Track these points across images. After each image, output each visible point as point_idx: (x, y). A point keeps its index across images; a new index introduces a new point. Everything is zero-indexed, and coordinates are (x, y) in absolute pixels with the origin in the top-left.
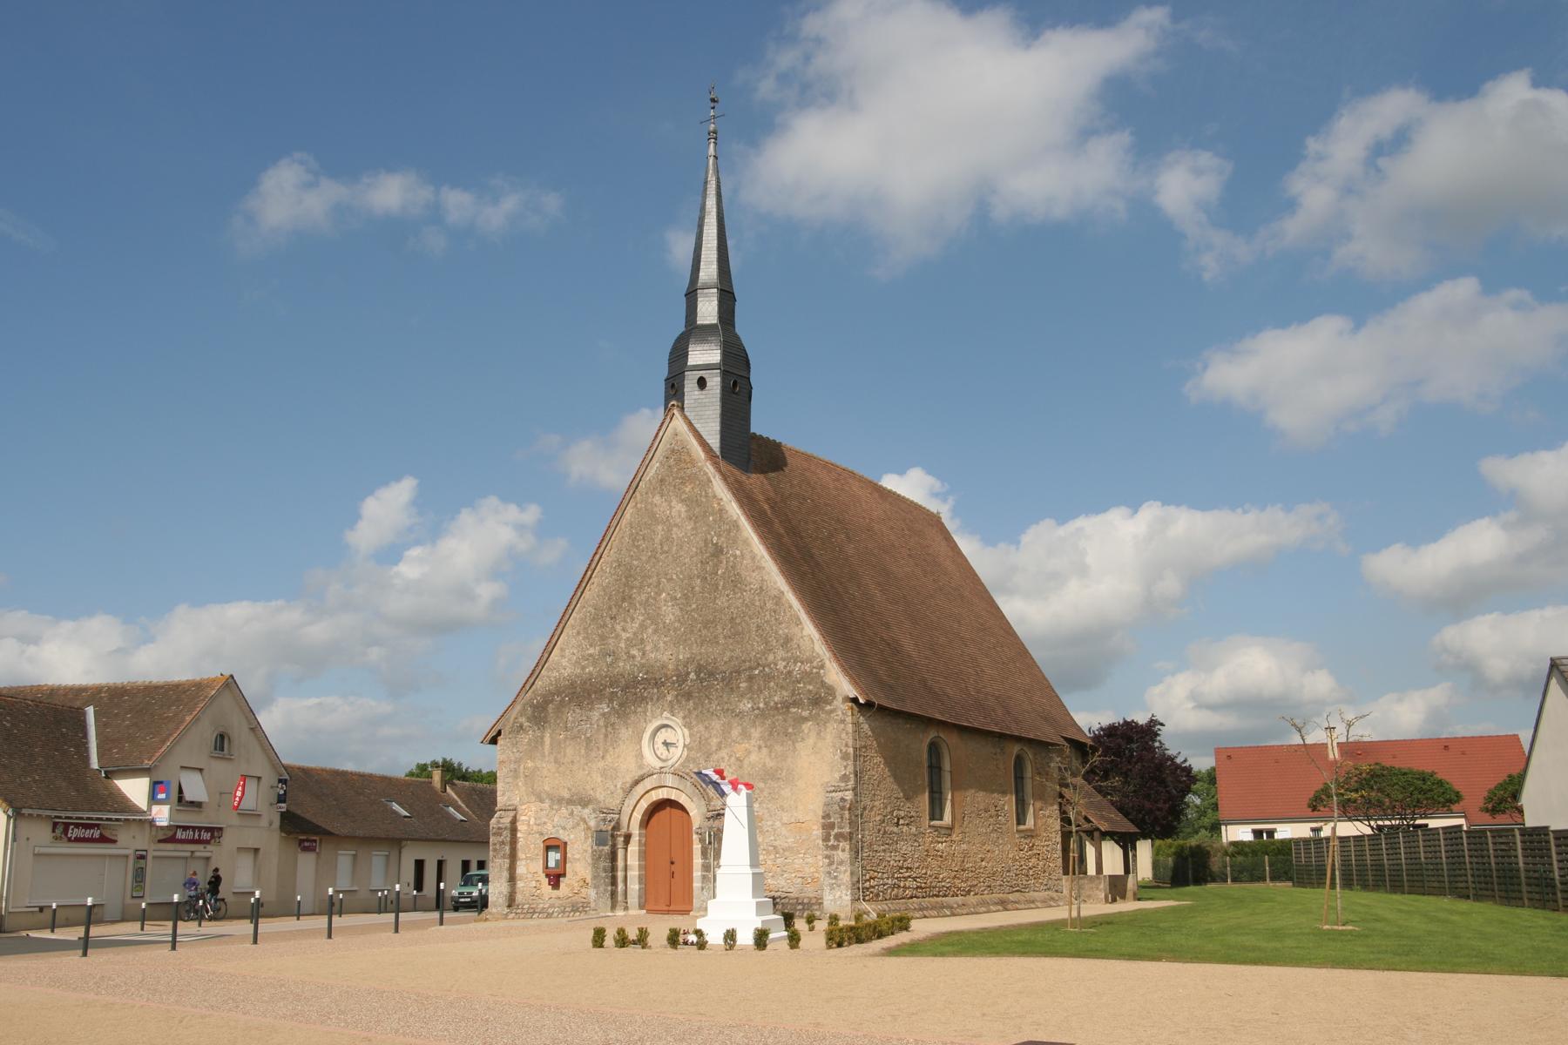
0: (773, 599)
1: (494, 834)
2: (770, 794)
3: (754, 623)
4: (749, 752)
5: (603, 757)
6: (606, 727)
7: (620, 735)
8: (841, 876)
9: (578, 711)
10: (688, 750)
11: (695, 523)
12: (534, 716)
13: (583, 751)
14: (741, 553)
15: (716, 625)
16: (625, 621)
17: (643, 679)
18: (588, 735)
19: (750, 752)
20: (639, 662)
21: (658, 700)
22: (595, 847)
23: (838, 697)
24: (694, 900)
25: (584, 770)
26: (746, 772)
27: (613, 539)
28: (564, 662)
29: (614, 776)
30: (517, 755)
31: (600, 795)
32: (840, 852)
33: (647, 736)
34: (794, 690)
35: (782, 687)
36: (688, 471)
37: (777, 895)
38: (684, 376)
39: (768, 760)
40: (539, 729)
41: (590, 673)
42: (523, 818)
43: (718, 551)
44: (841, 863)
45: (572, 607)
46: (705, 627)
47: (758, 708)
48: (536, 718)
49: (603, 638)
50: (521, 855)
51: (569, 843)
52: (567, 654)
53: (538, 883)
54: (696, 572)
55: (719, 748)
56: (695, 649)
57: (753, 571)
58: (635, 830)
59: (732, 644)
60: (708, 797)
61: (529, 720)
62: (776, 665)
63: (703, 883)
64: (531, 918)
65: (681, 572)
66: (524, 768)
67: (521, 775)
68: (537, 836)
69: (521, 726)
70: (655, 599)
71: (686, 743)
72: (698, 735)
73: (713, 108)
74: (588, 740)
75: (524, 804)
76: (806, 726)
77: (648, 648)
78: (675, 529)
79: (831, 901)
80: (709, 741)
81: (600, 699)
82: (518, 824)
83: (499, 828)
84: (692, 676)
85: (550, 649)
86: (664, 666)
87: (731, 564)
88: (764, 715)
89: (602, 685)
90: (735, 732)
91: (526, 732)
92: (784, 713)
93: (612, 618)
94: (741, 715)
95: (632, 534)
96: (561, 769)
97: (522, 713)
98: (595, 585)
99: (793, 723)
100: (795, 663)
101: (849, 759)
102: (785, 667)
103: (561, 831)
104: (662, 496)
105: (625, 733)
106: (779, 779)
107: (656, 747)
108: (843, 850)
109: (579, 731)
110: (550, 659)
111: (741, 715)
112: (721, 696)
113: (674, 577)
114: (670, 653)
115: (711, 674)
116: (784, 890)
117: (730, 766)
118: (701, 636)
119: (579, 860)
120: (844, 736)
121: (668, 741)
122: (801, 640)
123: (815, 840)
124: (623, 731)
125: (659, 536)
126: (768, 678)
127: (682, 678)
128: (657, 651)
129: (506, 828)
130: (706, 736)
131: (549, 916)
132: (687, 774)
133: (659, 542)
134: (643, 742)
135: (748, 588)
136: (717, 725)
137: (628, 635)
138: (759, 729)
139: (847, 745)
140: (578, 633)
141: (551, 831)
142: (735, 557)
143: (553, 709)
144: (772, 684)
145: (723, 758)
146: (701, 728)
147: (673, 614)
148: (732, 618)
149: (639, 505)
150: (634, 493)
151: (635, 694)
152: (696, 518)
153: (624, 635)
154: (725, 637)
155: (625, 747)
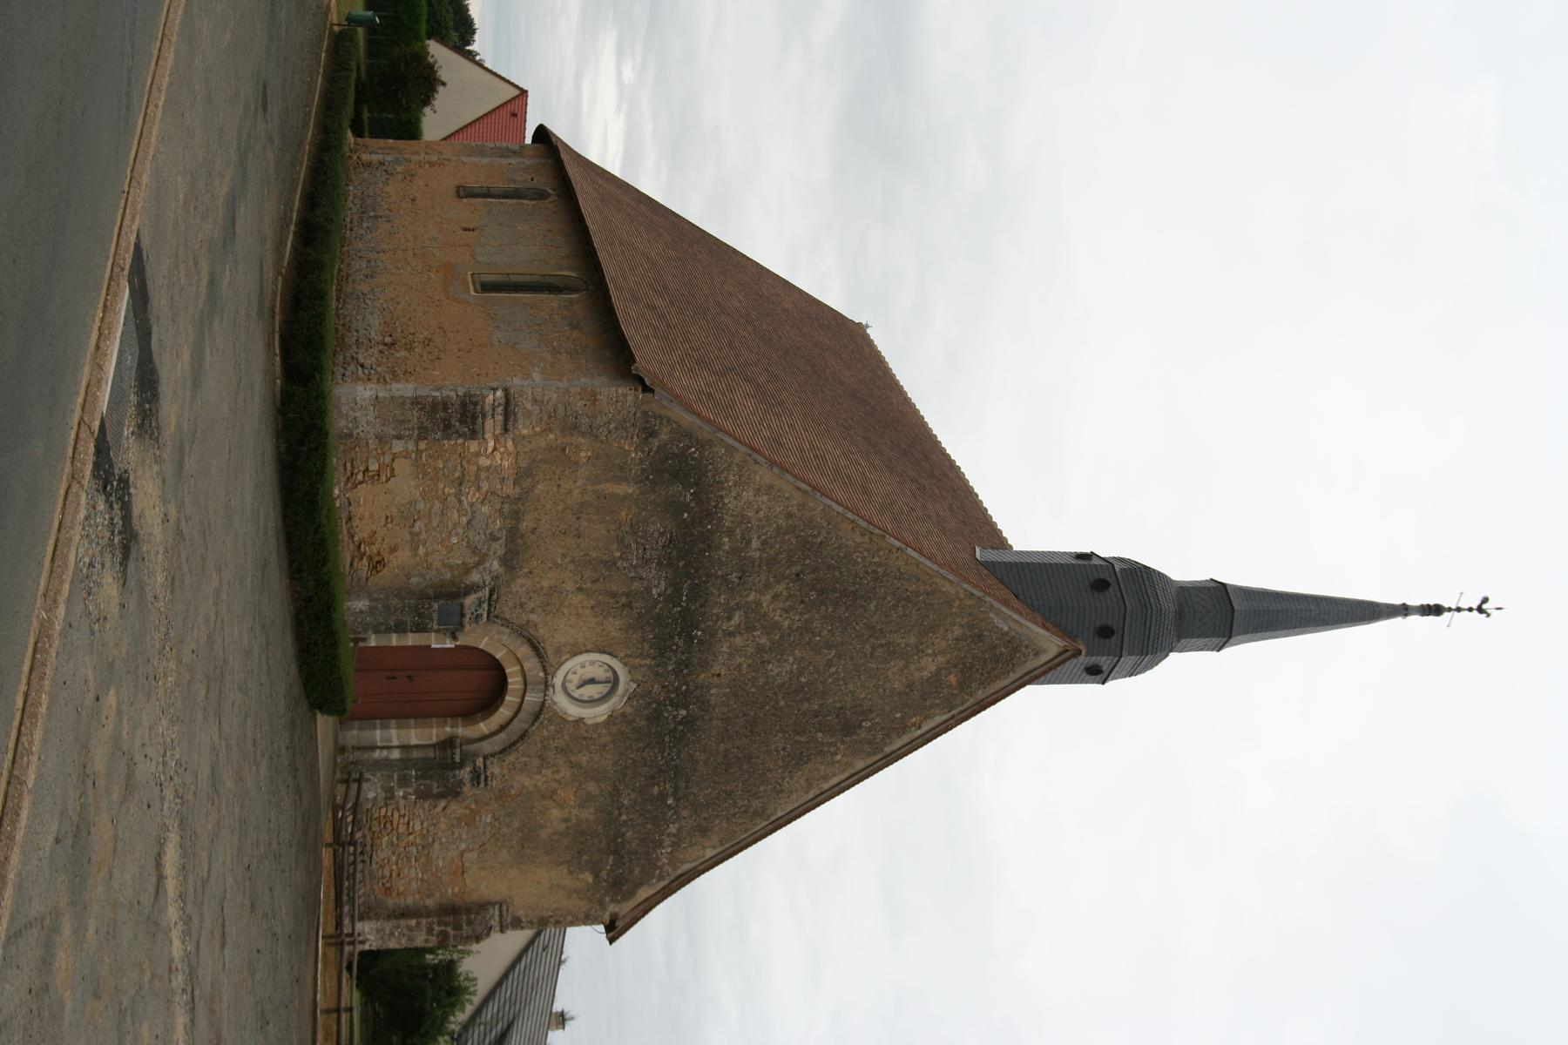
2: (504, 836)
4: (561, 806)
5: (580, 589)
6: (627, 595)
13: (594, 554)
15: (747, 737)
18: (619, 563)
20: (720, 627)
25: (564, 556)
29: (549, 608)
31: (520, 585)
39: (549, 830)
40: (643, 470)
43: (848, 729)
44: (411, 939)
47: (620, 814)
57: (807, 780)
69: (653, 434)
78: (902, 663)
80: (585, 752)
83: (474, 418)
84: (683, 712)
86: (705, 665)
93: (798, 575)
105: (613, 626)
106: (523, 846)
108: (426, 941)
113: (833, 670)
117: (546, 782)
119: (416, 554)
133: (891, 640)
134: (597, 654)
135: (786, 774)
137: (764, 605)
140: (789, 516)
144: (649, 826)
146: (606, 739)
147: (778, 675)
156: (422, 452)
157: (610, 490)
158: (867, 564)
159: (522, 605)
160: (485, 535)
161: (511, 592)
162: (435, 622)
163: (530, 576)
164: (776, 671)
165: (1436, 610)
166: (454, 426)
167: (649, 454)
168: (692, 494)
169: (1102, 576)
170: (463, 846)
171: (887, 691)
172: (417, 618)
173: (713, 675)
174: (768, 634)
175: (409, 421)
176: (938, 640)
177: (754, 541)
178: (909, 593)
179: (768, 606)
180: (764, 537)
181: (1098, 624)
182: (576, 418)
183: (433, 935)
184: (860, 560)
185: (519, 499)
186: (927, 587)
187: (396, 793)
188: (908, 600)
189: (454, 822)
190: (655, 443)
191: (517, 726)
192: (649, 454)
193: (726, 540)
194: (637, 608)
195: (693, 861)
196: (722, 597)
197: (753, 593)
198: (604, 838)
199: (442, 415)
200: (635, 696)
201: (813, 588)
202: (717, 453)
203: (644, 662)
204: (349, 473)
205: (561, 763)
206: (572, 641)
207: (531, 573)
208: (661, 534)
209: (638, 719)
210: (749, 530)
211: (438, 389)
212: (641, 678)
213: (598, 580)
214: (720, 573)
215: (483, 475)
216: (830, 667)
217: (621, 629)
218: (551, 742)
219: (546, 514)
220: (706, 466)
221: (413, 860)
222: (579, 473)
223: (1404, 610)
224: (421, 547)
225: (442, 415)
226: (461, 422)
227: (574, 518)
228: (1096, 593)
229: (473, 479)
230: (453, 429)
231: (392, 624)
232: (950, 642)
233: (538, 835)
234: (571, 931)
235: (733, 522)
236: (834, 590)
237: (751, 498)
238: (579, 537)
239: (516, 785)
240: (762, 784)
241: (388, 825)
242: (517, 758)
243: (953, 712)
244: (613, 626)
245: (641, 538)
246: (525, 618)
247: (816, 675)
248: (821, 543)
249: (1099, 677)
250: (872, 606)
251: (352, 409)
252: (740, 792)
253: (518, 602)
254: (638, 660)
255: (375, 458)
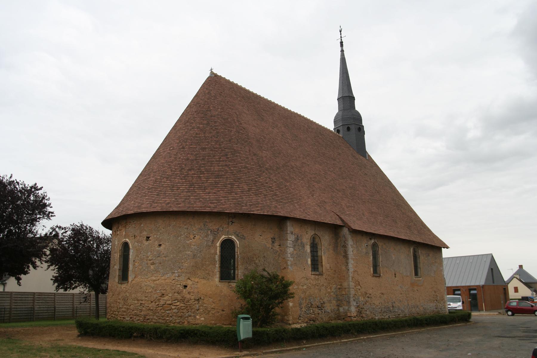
165: (342, 43)
169: (346, 128)
173: (345, 243)
211: (445, 290)
223: (342, 51)
228: (350, 131)
234: (482, 283)
249: (361, 127)
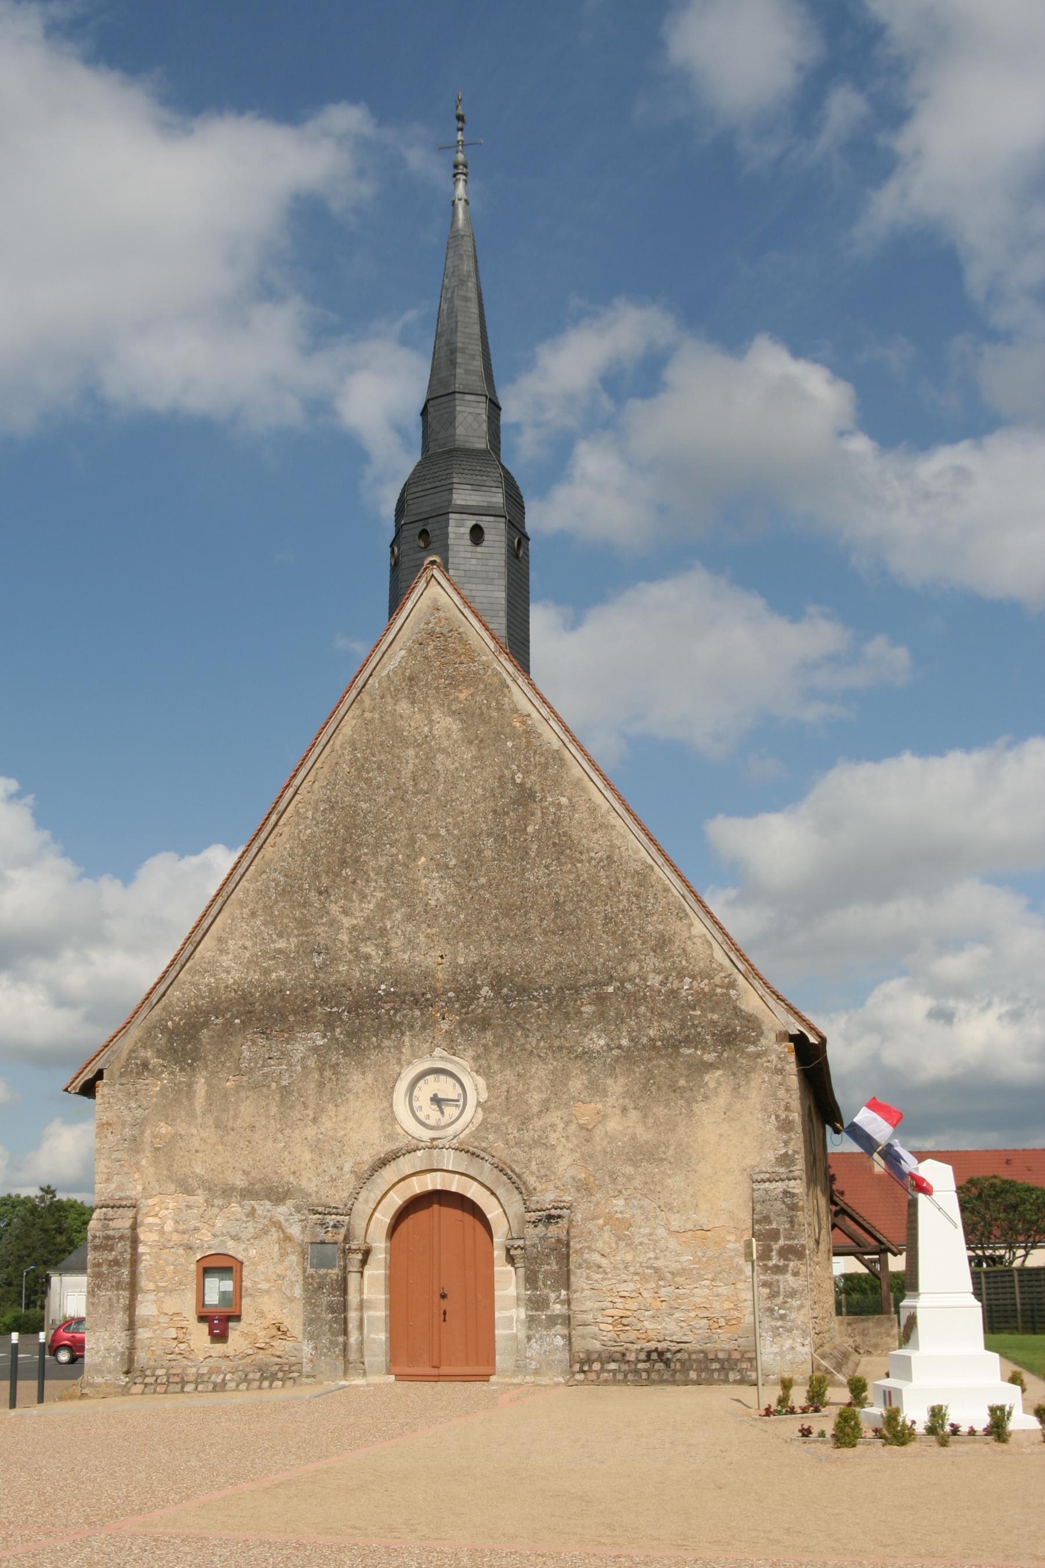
0: (633, 877)
1: (96, 1248)
3: (598, 913)
5: (315, 1120)
6: (321, 1070)
7: (351, 1084)
8: (793, 1315)
9: (261, 1041)
10: (484, 1110)
11: (480, 749)
12: (172, 1048)
13: (274, 1110)
14: (570, 800)
15: (526, 913)
16: (347, 897)
17: (388, 993)
18: (285, 1083)
19: (605, 1116)
20: (378, 966)
21: (424, 1027)
22: (311, 1271)
23: (766, 1032)
24: (497, 1358)
26: (599, 1148)
27: (318, 765)
28: (226, 961)
30: (139, 1113)
31: (309, 1182)
32: (789, 1277)
33: (402, 1087)
34: (683, 1021)
35: (662, 1015)
36: (463, 668)
37: (661, 1346)
38: (448, 520)
39: (639, 1130)
40: (182, 1070)
41: (281, 981)
42: (150, 1220)
43: (525, 797)
45: (241, 870)
46: (506, 915)
47: (619, 1047)
48: (175, 1051)
49: (303, 924)
50: (145, 1283)
51: (246, 1263)
52: (231, 948)
53: (180, 1332)
54: (484, 827)
55: (545, 1107)
56: (488, 949)
57: (595, 831)
58: (380, 1244)
59: (558, 944)
60: (527, 1189)
61: (160, 1053)
62: (645, 979)
63: (529, 1328)
64: (182, 1391)
65: (456, 825)
66: (154, 1137)
67: (147, 1147)
68: (181, 1251)
69: (145, 1065)
70: (405, 865)
71: (482, 1101)
72: (505, 1087)
73: (461, 129)
74: (285, 1092)
75: (151, 1196)
76: (711, 1078)
77: (395, 944)
78: (440, 757)
79: (776, 1354)
81: (309, 1023)
82: (139, 1230)
83: (108, 1238)
84: (485, 991)
85: (198, 938)
86: (427, 975)
87: (551, 817)
88: (629, 1057)
89: (306, 1000)
90: (577, 1084)
91: (154, 1073)
92: (670, 1056)
93: (321, 893)
94: (587, 1056)
95: (357, 759)
96: (229, 1138)
97: (146, 1041)
98: (284, 838)
99: (686, 1072)
100: (681, 976)
101: (791, 1129)
102: (663, 983)
103: (230, 1243)
104: (413, 703)
106: (662, 1160)
107: (415, 1104)
109: (265, 1076)
110: (197, 954)
111: (587, 1056)
112: (547, 1026)
113: (443, 832)
114: (439, 953)
115: (522, 990)
116: (674, 1338)
117: (567, 1138)
118: (498, 928)
119: (268, 1291)
120: (781, 1093)
121: (440, 1096)
122: (689, 943)
123: (731, 1258)
124: (355, 1077)
125: (410, 766)
126: (634, 999)
127: (466, 995)
128: (413, 948)
129: (122, 1238)
130: (520, 1088)
131: (219, 1387)
132: (484, 1150)
136: (540, 1071)
137: (355, 922)
138: (622, 1080)
139: (787, 1108)
140: (253, 914)
141: (208, 1242)
142: (559, 806)
143: (211, 1037)
145: (553, 1126)
148: (557, 903)
149: (368, 715)
150: (358, 694)
151: (378, 1017)
152: (481, 741)
153: (347, 922)
154: (545, 932)
155: (359, 1104)
156: (157, 1286)
157: (201, 1100)
158: (314, 823)
159: (333, 1180)
160: (248, 1221)
161: (317, 1192)
162: (330, 1271)
163: (298, 1173)
164: (438, 894)
166: (116, 1256)
167: (165, 1067)
168: (217, 1018)
170: (661, 1232)
171: (475, 764)
172: (325, 1291)
174: (391, 912)
175: (110, 1299)
176: (412, 724)
177: (278, 946)
178: (353, 770)
179: (356, 918)
180: (274, 937)
181: (469, 542)
182: (125, 1140)
183: (787, 1266)
184: (309, 831)
185: (210, 1189)
186: (346, 752)
187: (557, 1312)
188: (359, 770)
189: (622, 1244)
190: (155, 1061)
191: (488, 1174)
192: (165, 1067)
193: (274, 976)
194: (338, 1059)
195: (711, 946)
196: (341, 969)
197: (339, 937)
198: (654, 1062)
199: (104, 1269)
200: (452, 1048)
201: (338, 875)
202: (178, 999)
203: (407, 1044)
204: (179, 1357)
205: (541, 1123)
206: (378, 1124)
207: (294, 1173)
208: (254, 1042)
209: (484, 1041)
210: (265, 953)
212: (428, 1044)
213: (304, 1103)
214: (312, 976)
215: (182, 1227)
216: (439, 835)
217: (363, 1073)
218: (511, 1136)
219: (228, 1162)
220: (191, 1007)
221: (681, 1291)
222: (183, 1132)
224: (259, 1286)
225: (104, 1269)
226: (112, 1249)
227: (232, 1133)
229: (186, 1236)
230: (119, 1257)
231: (330, 1315)
232: (416, 709)
233: (647, 1142)
235: (255, 971)
236: (343, 851)
237: (230, 956)
238: (254, 1127)
239: (571, 1172)
240: (597, 884)
241: (625, 1321)
242: (532, 1173)
243: (509, 681)
244: (358, 1081)
245: (256, 1063)
246: (349, 1176)
247: (449, 850)
248: (286, 876)
250: (364, 805)
251: (97, 1352)
252: (608, 907)
253: (330, 1184)
254: (404, 1050)
255: (163, 1331)
